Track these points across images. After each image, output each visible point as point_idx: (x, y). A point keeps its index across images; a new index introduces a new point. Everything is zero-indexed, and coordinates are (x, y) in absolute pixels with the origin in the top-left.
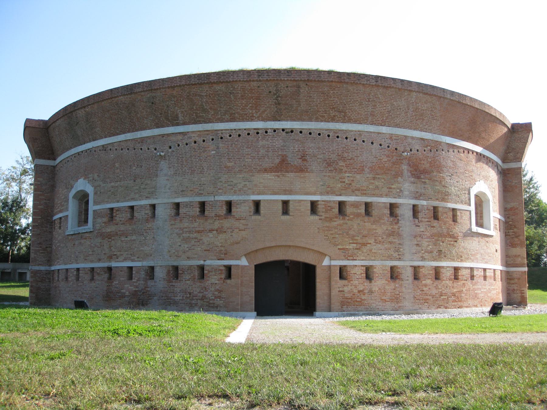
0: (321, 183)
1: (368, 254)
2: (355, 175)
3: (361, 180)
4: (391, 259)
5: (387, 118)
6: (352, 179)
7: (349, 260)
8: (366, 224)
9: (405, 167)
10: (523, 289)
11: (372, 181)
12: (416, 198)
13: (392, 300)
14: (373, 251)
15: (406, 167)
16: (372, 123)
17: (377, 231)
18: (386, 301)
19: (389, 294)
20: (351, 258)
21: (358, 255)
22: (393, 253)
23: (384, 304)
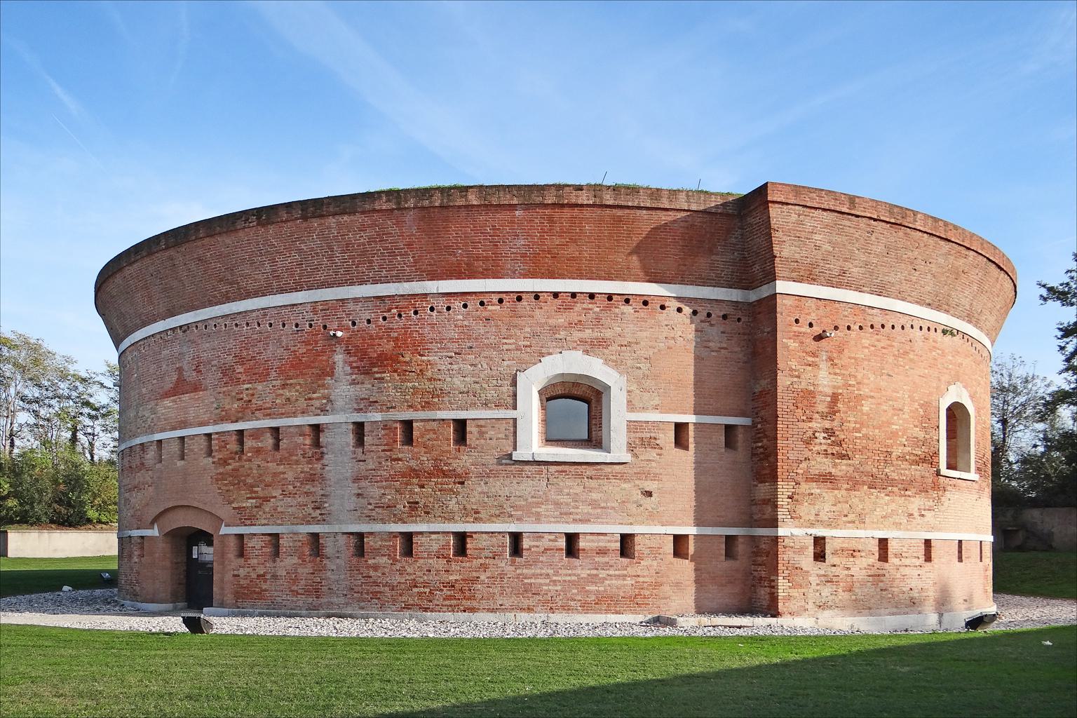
0: (215, 406)
1: (272, 515)
2: (256, 385)
3: (264, 391)
4: (308, 523)
5: (301, 276)
6: (251, 392)
7: (246, 525)
8: (270, 464)
9: (339, 358)
10: (772, 578)
11: (281, 392)
12: (359, 410)
13: (307, 592)
14: (279, 509)
15: (341, 356)
16: (282, 291)
17: (286, 476)
18: (298, 594)
19: (303, 582)
20: (249, 522)
21: (258, 516)
22: (312, 511)
23: (295, 599)
